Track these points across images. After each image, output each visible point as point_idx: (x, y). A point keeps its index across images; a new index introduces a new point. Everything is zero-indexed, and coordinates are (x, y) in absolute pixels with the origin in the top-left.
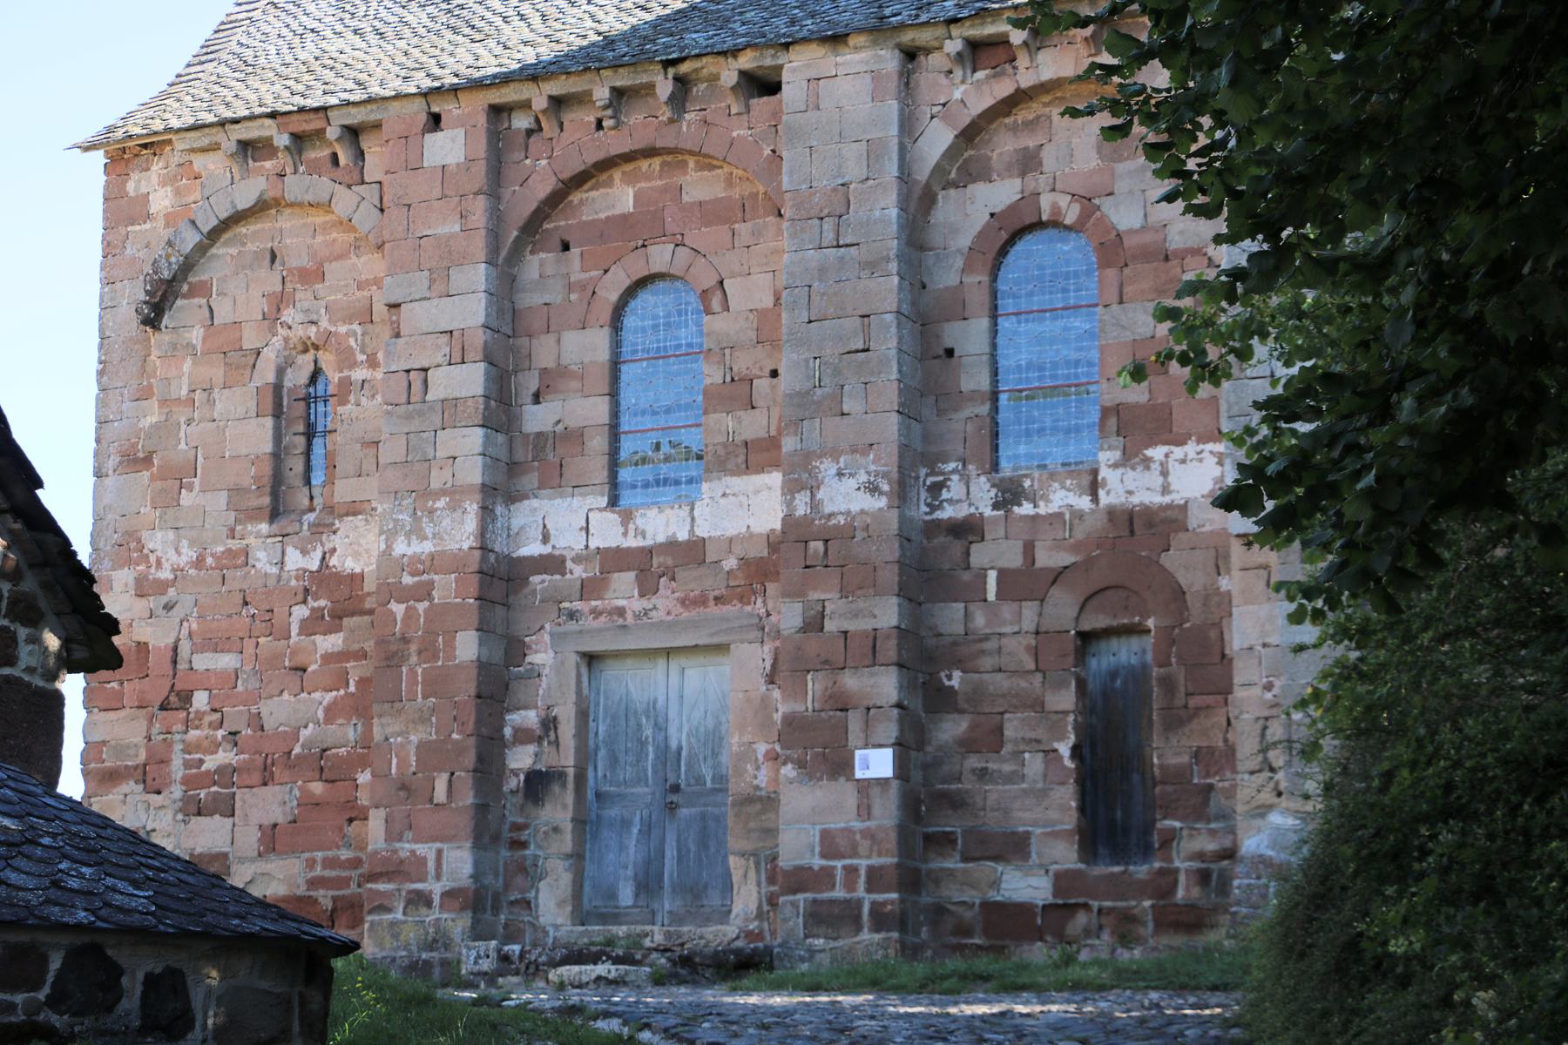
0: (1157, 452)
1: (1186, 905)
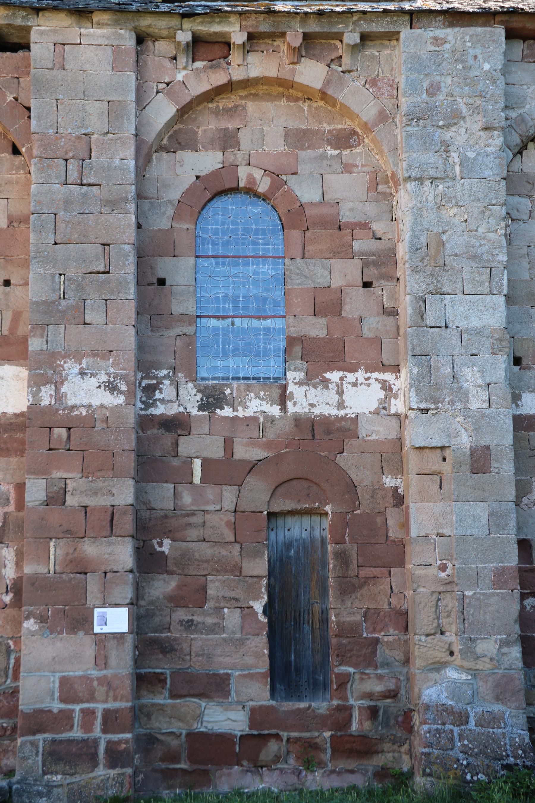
0: (334, 376)
1: (358, 736)
